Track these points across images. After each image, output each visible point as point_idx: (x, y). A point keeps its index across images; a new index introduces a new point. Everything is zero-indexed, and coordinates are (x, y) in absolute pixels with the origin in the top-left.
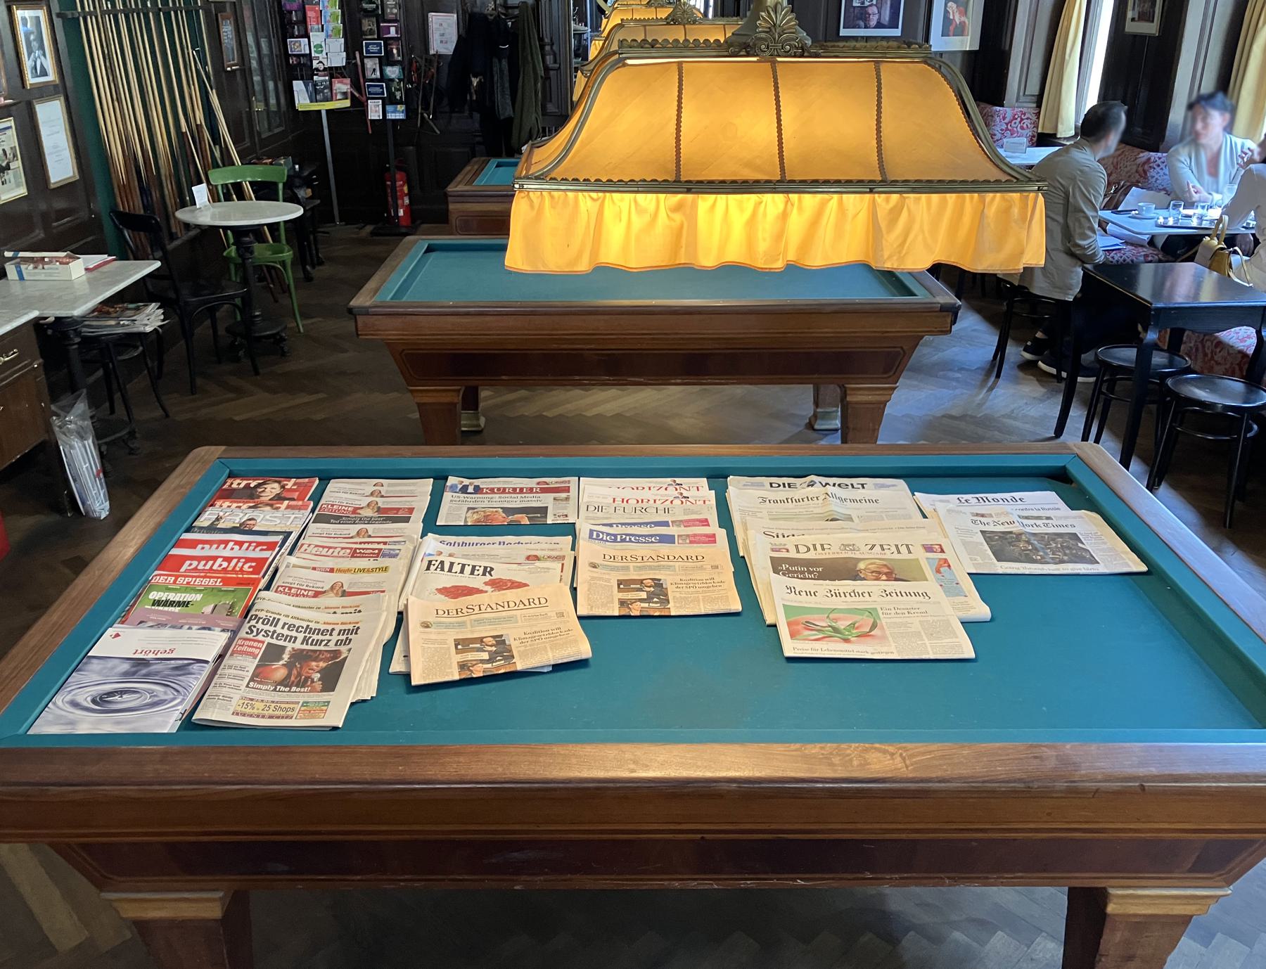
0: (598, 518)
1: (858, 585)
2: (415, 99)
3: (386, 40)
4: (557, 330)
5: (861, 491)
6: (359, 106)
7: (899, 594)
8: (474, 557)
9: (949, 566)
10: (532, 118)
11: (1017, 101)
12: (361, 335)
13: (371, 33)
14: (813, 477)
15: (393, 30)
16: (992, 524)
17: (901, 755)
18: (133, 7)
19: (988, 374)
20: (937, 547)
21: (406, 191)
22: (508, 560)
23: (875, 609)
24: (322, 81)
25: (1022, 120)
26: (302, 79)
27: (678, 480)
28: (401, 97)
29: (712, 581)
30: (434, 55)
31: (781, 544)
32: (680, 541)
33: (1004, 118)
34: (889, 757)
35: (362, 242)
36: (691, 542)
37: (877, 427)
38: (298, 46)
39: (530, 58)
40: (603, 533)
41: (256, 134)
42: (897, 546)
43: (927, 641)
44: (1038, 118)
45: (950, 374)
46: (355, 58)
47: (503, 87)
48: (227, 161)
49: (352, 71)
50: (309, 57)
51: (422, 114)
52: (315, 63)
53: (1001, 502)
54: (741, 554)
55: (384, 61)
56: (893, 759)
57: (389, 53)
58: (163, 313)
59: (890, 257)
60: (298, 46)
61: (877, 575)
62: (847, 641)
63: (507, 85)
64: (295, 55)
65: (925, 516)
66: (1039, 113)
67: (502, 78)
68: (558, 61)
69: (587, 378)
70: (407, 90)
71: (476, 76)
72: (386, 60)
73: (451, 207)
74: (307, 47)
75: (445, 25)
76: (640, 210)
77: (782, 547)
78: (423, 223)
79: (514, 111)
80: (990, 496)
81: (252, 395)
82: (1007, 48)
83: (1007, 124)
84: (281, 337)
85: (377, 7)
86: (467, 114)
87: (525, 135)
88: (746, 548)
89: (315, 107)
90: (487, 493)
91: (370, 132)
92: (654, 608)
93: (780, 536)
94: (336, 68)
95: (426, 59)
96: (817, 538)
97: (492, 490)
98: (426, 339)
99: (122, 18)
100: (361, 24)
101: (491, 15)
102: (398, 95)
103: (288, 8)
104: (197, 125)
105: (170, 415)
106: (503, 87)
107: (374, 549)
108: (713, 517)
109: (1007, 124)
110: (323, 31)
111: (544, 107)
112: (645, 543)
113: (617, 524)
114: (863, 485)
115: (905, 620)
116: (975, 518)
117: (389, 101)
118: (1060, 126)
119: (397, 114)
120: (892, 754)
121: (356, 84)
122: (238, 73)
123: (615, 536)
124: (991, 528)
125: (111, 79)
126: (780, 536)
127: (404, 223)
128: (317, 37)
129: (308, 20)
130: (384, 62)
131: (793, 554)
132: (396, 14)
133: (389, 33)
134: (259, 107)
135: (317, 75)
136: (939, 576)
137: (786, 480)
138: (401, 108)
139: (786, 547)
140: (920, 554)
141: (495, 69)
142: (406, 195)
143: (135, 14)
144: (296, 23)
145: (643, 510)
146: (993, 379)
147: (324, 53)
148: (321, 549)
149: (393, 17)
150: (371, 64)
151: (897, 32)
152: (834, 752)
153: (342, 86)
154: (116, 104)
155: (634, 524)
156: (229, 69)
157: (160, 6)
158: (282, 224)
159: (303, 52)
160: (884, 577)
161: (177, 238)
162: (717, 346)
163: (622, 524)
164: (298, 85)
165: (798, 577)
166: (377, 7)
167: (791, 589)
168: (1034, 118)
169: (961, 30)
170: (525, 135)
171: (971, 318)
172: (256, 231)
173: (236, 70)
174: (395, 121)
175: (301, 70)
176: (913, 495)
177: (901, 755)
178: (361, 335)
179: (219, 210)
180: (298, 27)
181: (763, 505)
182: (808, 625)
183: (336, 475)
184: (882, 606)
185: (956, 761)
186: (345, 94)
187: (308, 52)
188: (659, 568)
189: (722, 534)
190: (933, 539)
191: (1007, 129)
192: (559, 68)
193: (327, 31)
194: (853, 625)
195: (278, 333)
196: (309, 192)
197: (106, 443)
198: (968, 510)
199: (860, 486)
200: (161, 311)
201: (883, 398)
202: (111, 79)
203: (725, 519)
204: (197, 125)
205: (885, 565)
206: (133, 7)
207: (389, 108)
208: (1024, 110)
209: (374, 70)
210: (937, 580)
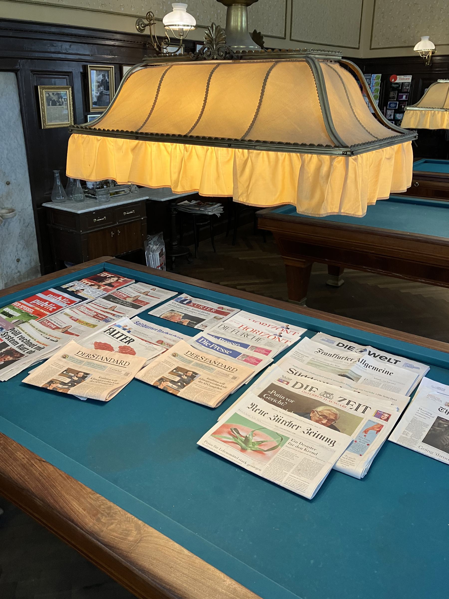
3: (400, 102)
13: (394, 98)
15: (404, 97)
58: (223, 209)
69: (370, 268)
76: (83, 137)
112: (222, 353)
114: (397, 361)
115: (293, 452)
133: (402, 98)
166: (399, 86)
167: (377, 420)
197: (175, 257)
209: (391, 115)
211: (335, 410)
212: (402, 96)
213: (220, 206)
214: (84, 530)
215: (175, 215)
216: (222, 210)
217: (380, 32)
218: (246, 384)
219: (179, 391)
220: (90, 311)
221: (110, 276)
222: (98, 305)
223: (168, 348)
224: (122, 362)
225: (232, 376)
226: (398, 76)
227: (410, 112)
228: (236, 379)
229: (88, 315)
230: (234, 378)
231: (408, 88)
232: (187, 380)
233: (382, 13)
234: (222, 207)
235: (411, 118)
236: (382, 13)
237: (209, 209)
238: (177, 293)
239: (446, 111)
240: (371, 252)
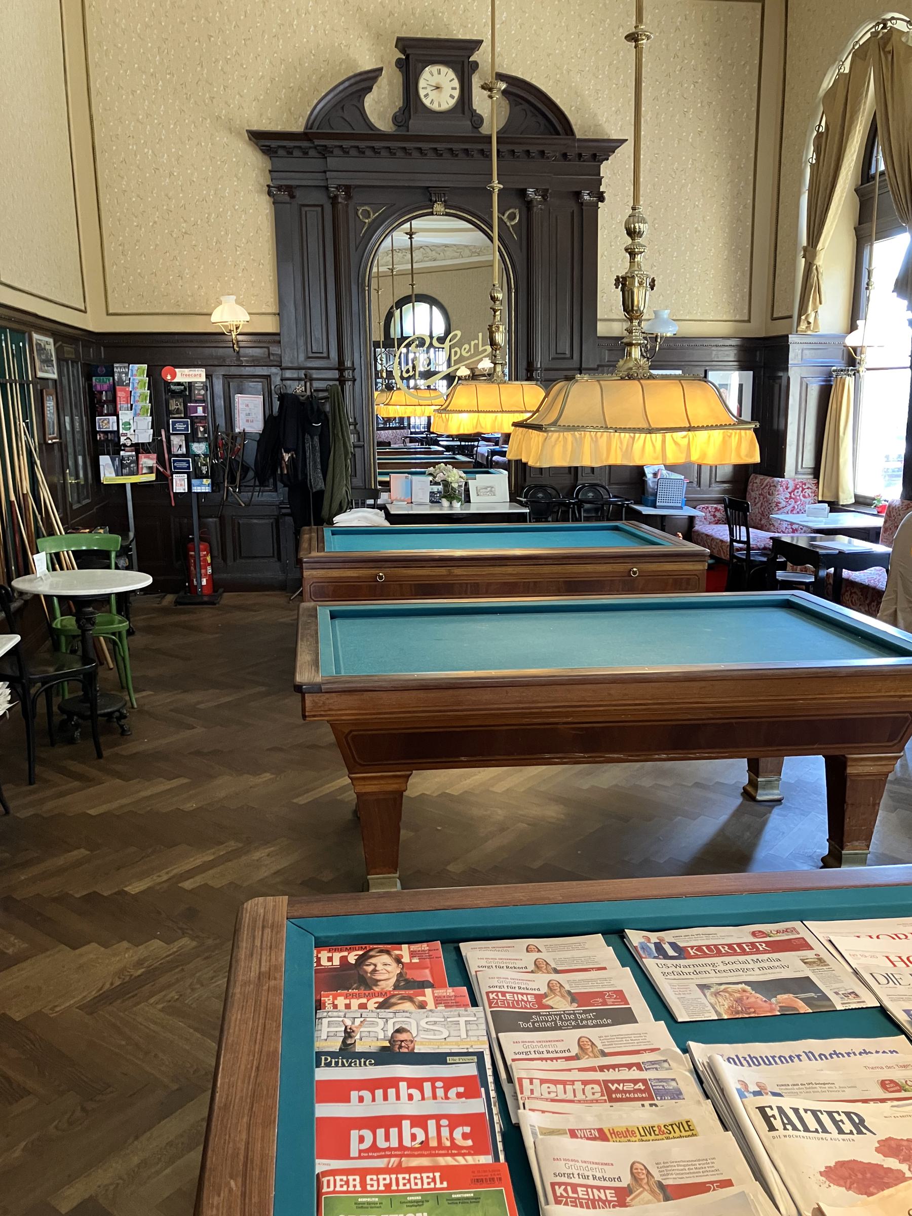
3: (191, 418)
4: (533, 702)
6: (164, 480)
10: (343, 491)
12: (309, 716)
15: (200, 409)
21: (209, 562)
24: (129, 456)
25: (803, 489)
28: (207, 472)
33: (787, 488)
35: (165, 611)
37: (877, 802)
38: (106, 423)
44: (818, 487)
46: (161, 436)
47: (315, 463)
49: (156, 447)
50: (117, 433)
51: (227, 487)
52: (123, 440)
55: (190, 438)
57: (195, 431)
58: (10, 694)
60: (106, 423)
64: (103, 432)
66: (818, 483)
69: (558, 756)
70: (212, 465)
72: (191, 438)
73: (306, 573)
75: (251, 406)
78: (224, 592)
81: (100, 784)
82: (783, 428)
83: (790, 493)
84: (121, 714)
85: (185, 388)
87: (335, 506)
91: (173, 505)
94: (143, 444)
98: (385, 718)
101: (303, 396)
102: (204, 470)
103: (99, 388)
104: (23, 494)
105: (11, 811)
106: (315, 463)
109: (790, 493)
110: (131, 410)
118: (841, 494)
119: (203, 486)
121: (160, 460)
122: (56, 446)
127: (205, 592)
128: (125, 416)
129: (118, 399)
130: (190, 438)
132: (203, 395)
134: (71, 480)
138: (207, 482)
141: (307, 445)
142: (209, 565)
144: (105, 402)
153: (148, 461)
156: (50, 442)
158: (113, 597)
159: (111, 429)
162: (711, 715)
168: (814, 488)
170: (335, 506)
172: (101, 601)
173: (54, 443)
175: (108, 446)
178: (309, 716)
179: (58, 579)
180: (107, 406)
183: (464, 936)
187: (116, 429)
191: (791, 498)
193: (135, 410)
195: (118, 711)
200: (8, 691)
201: (885, 769)
204: (23, 494)
207: (194, 481)
208: (804, 481)
209: (180, 446)
217: (123, 282)
226: (177, 370)
227: (552, 435)
233: (120, 245)
235: (554, 446)
236: (120, 245)
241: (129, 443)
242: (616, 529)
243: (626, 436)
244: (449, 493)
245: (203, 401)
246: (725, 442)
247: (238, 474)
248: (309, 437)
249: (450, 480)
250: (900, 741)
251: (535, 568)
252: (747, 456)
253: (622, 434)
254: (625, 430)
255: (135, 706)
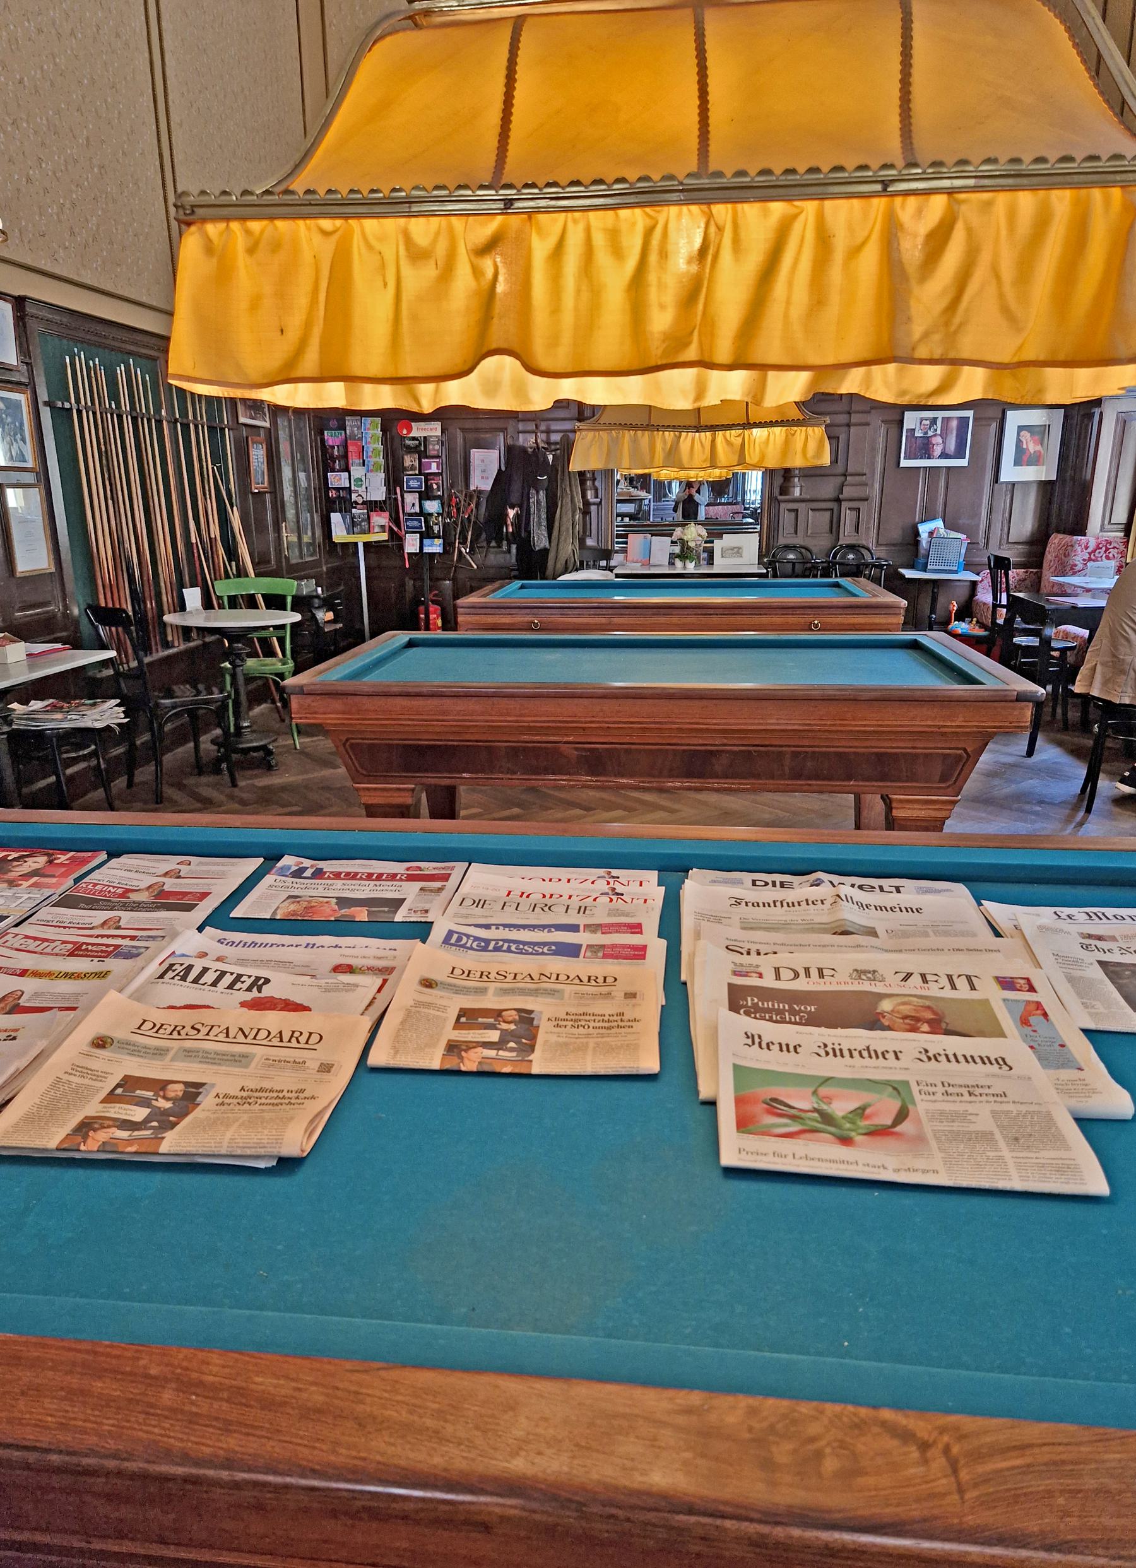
0: (474, 916)
1: (878, 1039)
2: (453, 533)
3: (427, 476)
5: (895, 895)
6: (397, 539)
7: (952, 1058)
8: (242, 962)
9: (1045, 1015)
11: (1101, 530)
13: (412, 468)
14: (821, 875)
15: (434, 466)
16: (1116, 950)
17: (947, 1450)
18: (144, 411)
19: (1075, 808)
20: (1022, 982)
22: (305, 971)
23: (906, 1083)
25: (1107, 549)
26: (340, 511)
27: (615, 872)
28: (439, 531)
29: (619, 1018)
30: (474, 491)
31: (751, 965)
32: (588, 954)
34: (915, 1455)
36: (605, 956)
38: (337, 480)
39: (568, 490)
40: (468, 936)
41: (284, 560)
42: (950, 977)
43: (1006, 1153)
44: (1127, 547)
45: (1027, 807)
46: (396, 494)
48: (241, 573)
49: (390, 505)
50: (349, 490)
53: (1129, 920)
54: (683, 978)
55: (424, 495)
56: (925, 1462)
57: (428, 487)
58: (123, 712)
59: (926, 335)
61: (912, 1024)
62: (846, 1141)
63: (544, 516)
64: (334, 488)
65: (997, 934)
66: (1128, 541)
67: (539, 510)
68: (600, 496)
70: (445, 525)
71: (512, 507)
72: (426, 495)
74: (348, 481)
77: (752, 969)
79: (550, 542)
80: (1110, 911)
82: (1088, 477)
83: (1090, 554)
85: (420, 444)
86: (505, 548)
88: (692, 973)
89: (351, 539)
90: (329, 878)
92: (506, 1060)
93: (753, 953)
95: (466, 494)
96: (814, 959)
97: (337, 876)
99: (128, 422)
100: (403, 459)
102: (436, 529)
103: (331, 444)
104: (210, 539)
107: (107, 946)
108: (651, 924)
109: (1090, 554)
110: (364, 465)
111: (582, 542)
112: (531, 954)
113: (497, 926)
116: (1087, 941)
117: (427, 534)
119: (435, 547)
120: (924, 1446)
121: (396, 520)
123: (487, 942)
124: (1116, 957)
125: (106, 476)
126: (753, 953)
128: (357, 471)
129: (350, 454)
131: (769, 982)
132: (438, 450)
135: (355, 508)
136: (1027, 1030)
137: (778, 878)
139: (760, 970)
140: (996, 997)
143: (145, 420)
145: (546, 909)
146: (1081, 814)
147: (364, 487)
148: (30, 941)
149: (435, 453)
150: (411, 499)
151: (964, 462)
152: (780, 1426)
153: (381, 519)
154: (110, 502)
155: (524, 927)
157: (178, 416)
160: (925, 1027)
161: (173, 647)
163: (505, 926)
164: (336, 518)
165: (771, 1020)
166: (420, 444)
167: (753, 1039)
168: (1122, 547)
169: (1036, 460)
170: (560, 566)
171: (1053, 751)
174: (432, 555)
176: (980, 904)
177: (947, 1450)
181: (735, 909)
182: (774, 1106)
184: (919, 1078)
185: (1090, 1483)
186: (383, 527)
188: (535, 993)
189: (658, 948)
190: (1018, 968)
192: (601, 502)
194: (861, 1112)
196: (330, 616)
198: (1073, 928)
199: (893, 889)
202: (106, 476)
203: (670, 925)
205: (929, 1008)
206: (144, 411)
207: (426, 541)
209: (414, 505)
210: (1025, 1038)
211: (915, 999)
212: (430, 463)
213: (116, 706)
214: (756, 1516)
215: (5, 736)
216: (122, 715)
218: (664, 1003)
219: (163, 1138)
220: (46, 944)
221: (14, 855)
222: (55, 926)
223: (386, 977)
224: (297, 1034)
225: (316, 1065)
228: (333, 1070)
229: (57, 955)
230: (326, 1068)
231: (437, 447)
232: (177, 1109)
234: (122, 709)
237: (92, 715)
238: (262, 860)
239: (658, 430)
240: (565, 739)
241: (360, 501)
242: (837, 585)
243: (669, 436)
244: (685, 553)
245: (438, 457)
246: (787, 443)
247: (470, 533)
248: (534, 492)
249: (685, 538)
250: (955, 782)
251: (702, 618)
252: (814, 457)
253: (667, 433)
254: (666, 428)
255: (298, 747)
